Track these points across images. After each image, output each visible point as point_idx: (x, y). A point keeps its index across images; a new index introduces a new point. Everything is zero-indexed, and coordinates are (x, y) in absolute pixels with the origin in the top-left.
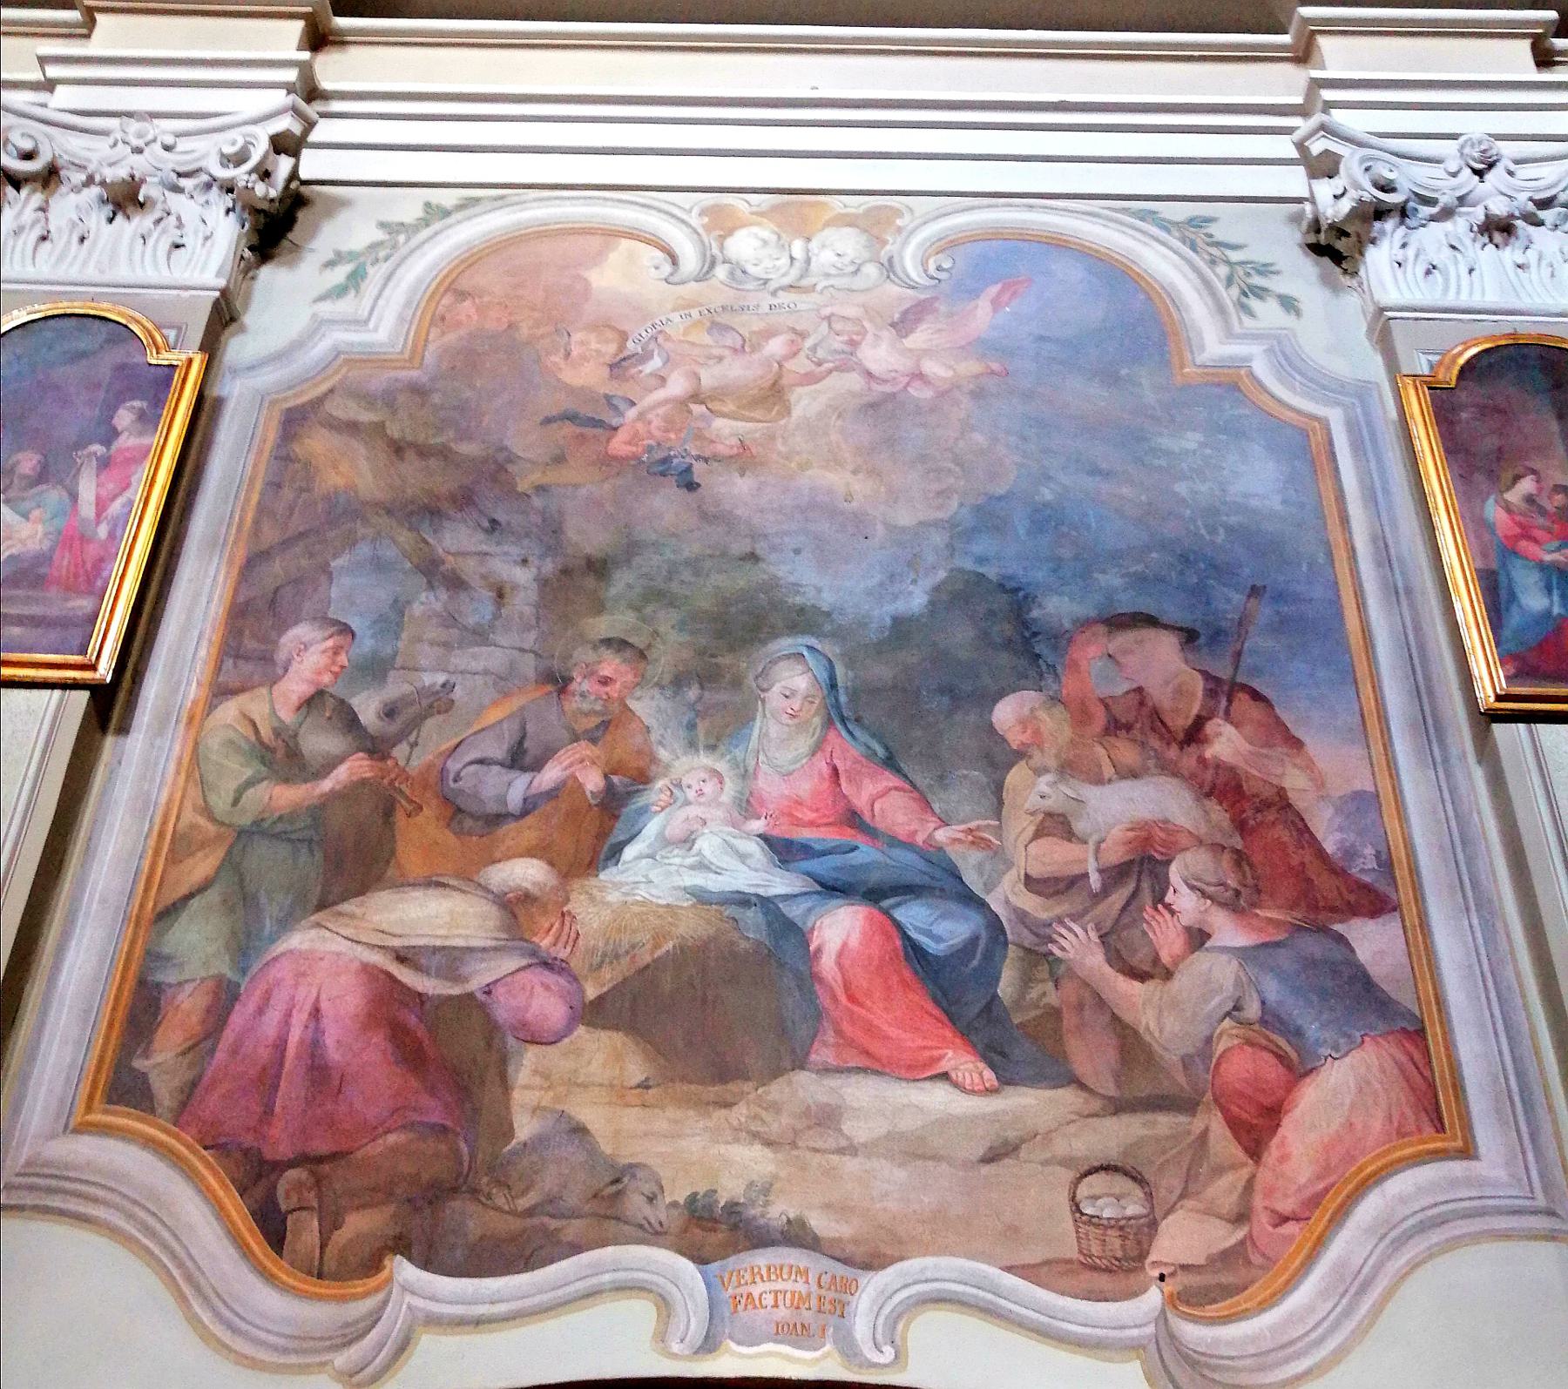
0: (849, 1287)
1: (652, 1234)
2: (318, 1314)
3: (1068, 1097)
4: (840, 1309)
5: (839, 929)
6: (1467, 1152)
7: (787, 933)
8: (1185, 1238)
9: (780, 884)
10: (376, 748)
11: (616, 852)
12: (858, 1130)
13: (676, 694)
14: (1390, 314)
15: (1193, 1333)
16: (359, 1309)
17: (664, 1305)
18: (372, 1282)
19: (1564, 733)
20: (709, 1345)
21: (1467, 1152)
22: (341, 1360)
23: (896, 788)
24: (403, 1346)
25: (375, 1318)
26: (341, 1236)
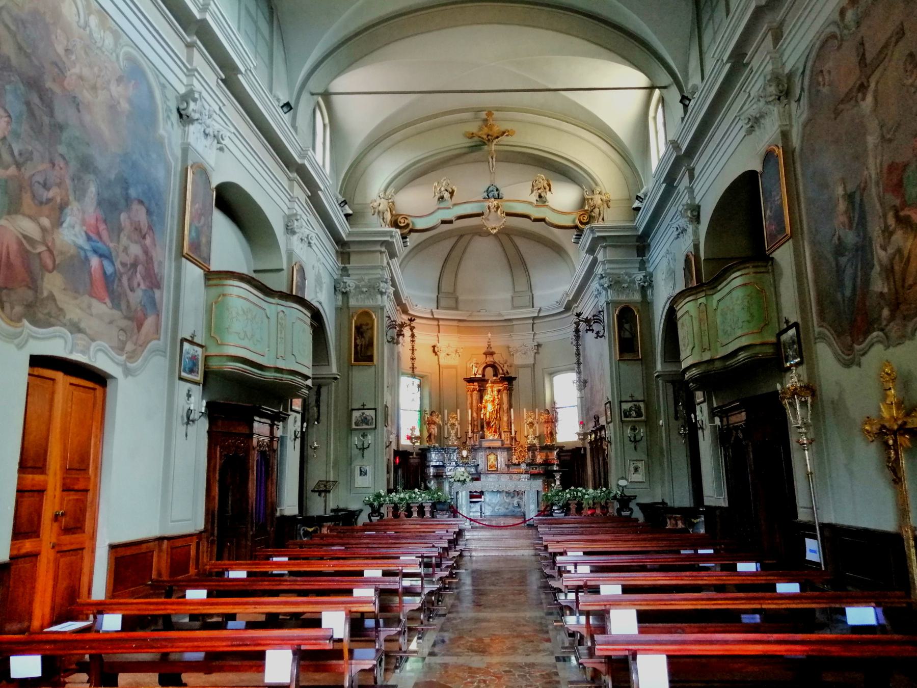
0: (90, 345)
1: (64, 325)
2: (11, 329)
3: (120, 313)
4: (88, 349)
5: (95, 261)
6: (159, 339)
7: (87, 259)
8: (129, 347)
9: (87, 247)
10: (19, 166)
11: (62, 224)
12: (94, 311)
13: (541, 587)
14: (196, 74)
15: (128, 364)
16: (19, 330)
17: (66, 342)
18: (18, 325)
19: (833, 517)
20: (71, 352)
21: (159, 339)
22: (16, 341)
23: (316, 317)
24: (27, 341)
25: (21, 333)
26: (14, 311)
